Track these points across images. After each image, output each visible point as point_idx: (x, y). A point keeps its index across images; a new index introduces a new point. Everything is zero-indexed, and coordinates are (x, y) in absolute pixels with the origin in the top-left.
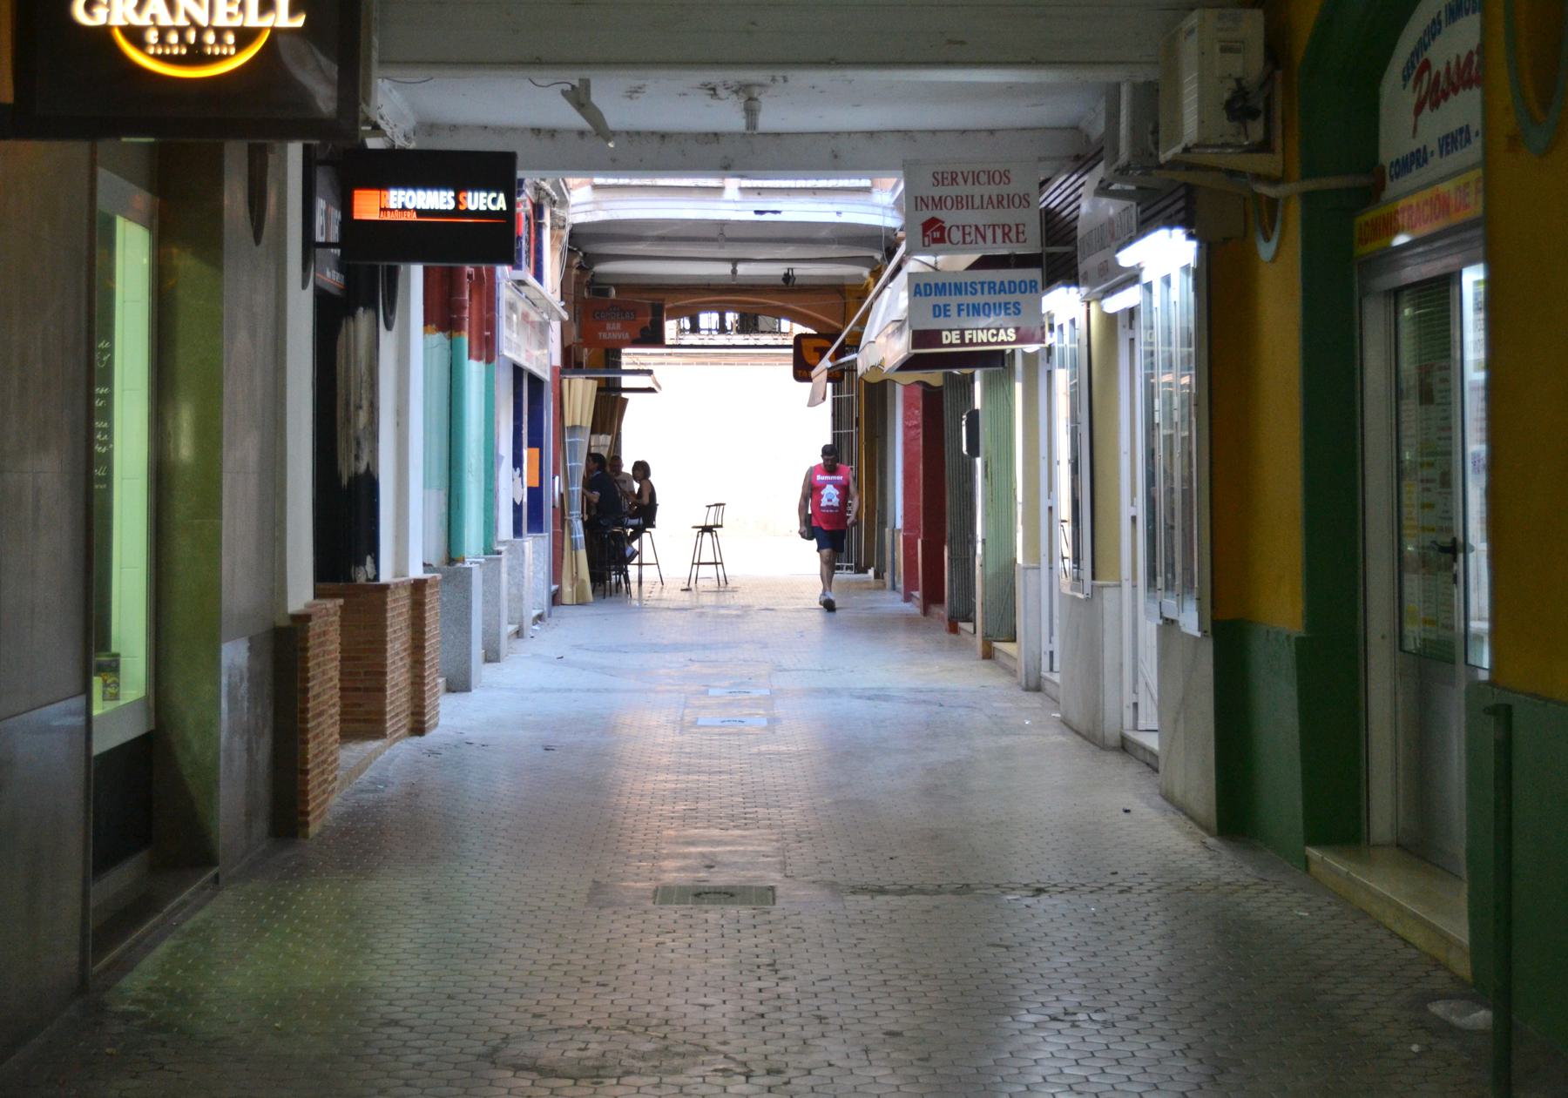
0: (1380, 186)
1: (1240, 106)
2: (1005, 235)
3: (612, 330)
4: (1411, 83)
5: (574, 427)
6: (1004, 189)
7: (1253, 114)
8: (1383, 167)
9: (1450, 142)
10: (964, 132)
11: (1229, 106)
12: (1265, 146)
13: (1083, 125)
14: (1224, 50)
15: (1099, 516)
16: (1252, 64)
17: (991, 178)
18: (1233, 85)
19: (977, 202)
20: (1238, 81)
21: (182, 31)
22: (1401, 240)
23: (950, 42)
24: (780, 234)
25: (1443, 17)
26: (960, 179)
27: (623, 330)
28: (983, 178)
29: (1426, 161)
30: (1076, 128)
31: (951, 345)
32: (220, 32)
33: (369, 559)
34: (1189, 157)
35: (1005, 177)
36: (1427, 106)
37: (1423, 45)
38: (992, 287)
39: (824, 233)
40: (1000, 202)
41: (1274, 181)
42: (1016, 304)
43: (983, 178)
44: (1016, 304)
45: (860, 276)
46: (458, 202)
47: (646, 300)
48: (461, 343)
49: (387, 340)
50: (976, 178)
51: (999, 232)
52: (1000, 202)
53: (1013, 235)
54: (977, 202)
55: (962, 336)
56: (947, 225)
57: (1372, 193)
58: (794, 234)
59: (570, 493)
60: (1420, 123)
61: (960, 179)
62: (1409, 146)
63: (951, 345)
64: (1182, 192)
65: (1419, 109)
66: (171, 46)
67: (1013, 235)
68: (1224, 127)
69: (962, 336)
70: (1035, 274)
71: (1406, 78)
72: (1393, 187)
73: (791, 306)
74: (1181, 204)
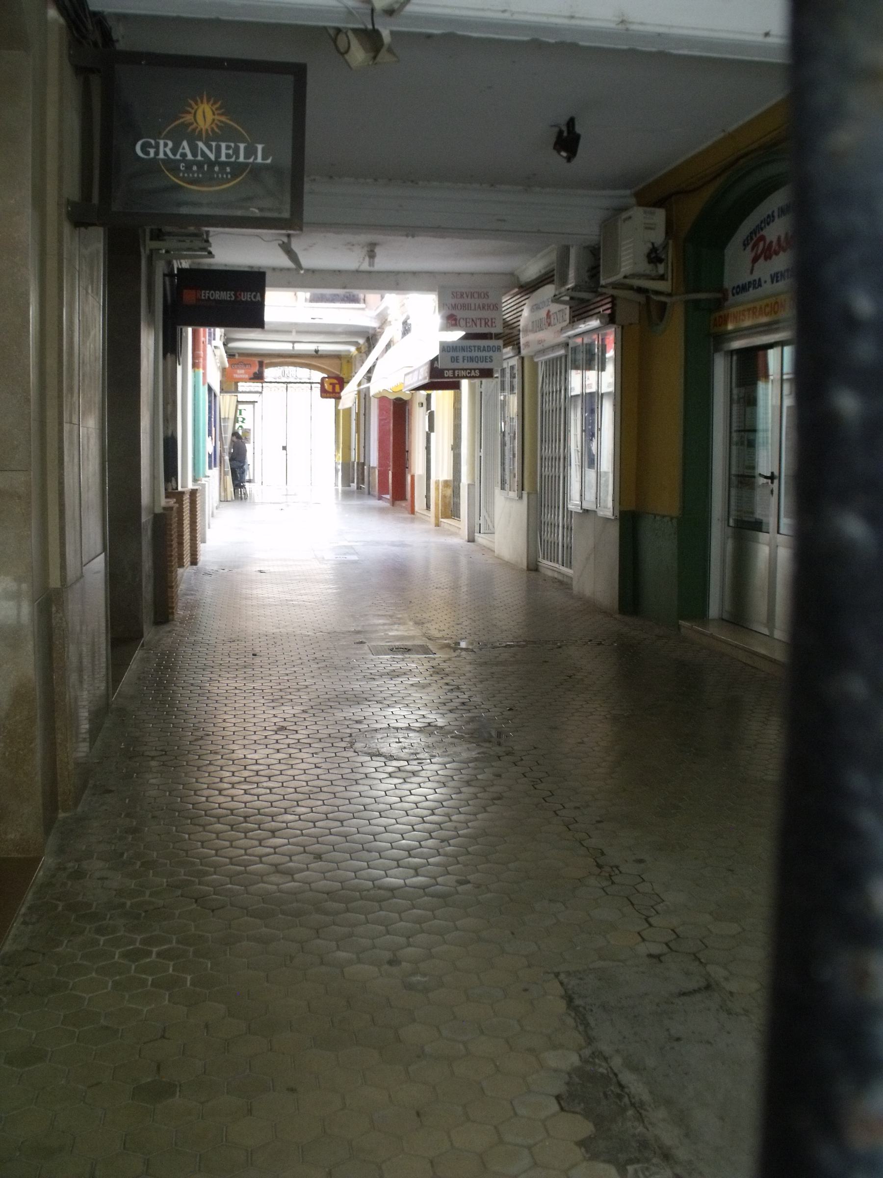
0: (725, 299)
1: (654, 256)
2: (486, 323)
3: (241, 372)
4: (749, 247)
5: (225, 419)
6: (485, 301)
7: (660, 261)
8: (727, 290)
9: (775, 278)
10: (459, 274)
11: (648, 256)
12: (662, 278)
13: (516, 273)
14: (646, 228)
15: (778, 454)
16: (658, 236)
17: (479, 296)
18: (651, 246)
19: (473, 307)
20: (653, 244)
21: (200, 165)
22: (730, 327)
23: (498, 220)
24: (306, 329)
25: (776, 214)
26: (465, 295)
27: (246, 373)
28: (476, 296)
29: (760, 285)
30: (512, 274)
31: (448, 377)
32: (223, 165)
33: (173, 479)
34: (628, 281)
35: (486, 295)
36: (762, 258)
37: (759, 228)
38: (479, 348)
39: (339, 330)
40: (483, 308)
41: (669, 295)
42: (491, 357)
43: (476, 296)
44: (491, 357)
45: (349, 351)
46: (236, 297)
47: (257, 360)
48: (199, 374)
49: (179, 369)
50: (472, 296)
51: (483, 322)
52: (483, 308)
53: (489, 324)
54: (473, 307)
55: (454, 374)
56: (458, 317)
57: (719, 304)
58: (310, 329)
59: (224, 449)
60: (755, 268)
61: (465, 295)
62: (746, 278)
63: (448, 377)
64: (609, 300)
65: (755, 260)
66: (193, 173)
67: (489, 324)
68: (644, 267)
69: (454, 374)
70: (500, 343)
71: (745, 245)
72: (731, 299)
73: (314, 363)
74: (609, 306)
